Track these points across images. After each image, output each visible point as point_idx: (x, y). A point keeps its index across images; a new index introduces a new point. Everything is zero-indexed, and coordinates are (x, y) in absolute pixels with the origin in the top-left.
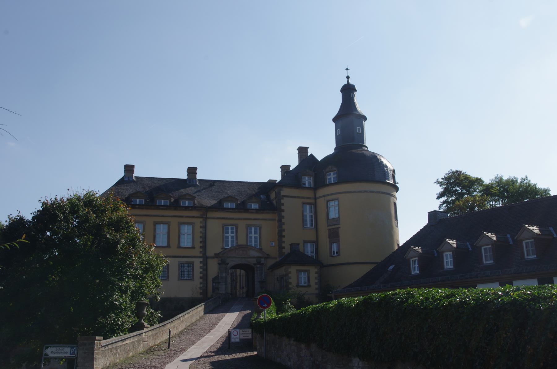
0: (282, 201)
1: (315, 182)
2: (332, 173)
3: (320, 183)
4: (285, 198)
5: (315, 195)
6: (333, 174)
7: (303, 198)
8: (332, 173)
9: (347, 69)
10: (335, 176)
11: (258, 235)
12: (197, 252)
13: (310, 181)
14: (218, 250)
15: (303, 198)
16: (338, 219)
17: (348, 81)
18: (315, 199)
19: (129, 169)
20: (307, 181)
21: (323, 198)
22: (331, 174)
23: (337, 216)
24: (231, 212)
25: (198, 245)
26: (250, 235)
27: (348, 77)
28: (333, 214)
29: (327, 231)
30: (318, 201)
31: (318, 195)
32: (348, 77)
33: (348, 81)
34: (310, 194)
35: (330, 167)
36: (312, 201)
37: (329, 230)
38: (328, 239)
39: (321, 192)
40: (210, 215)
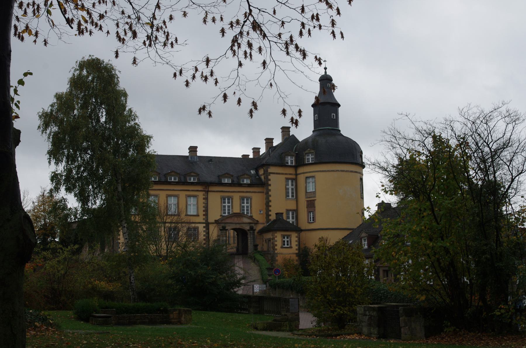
3: (300, 163)
7: (286, 174)
12: (201, 219)
14: (218, 217)
15: (286, 174)
16: (314, 193)
17: (326, 72)
18: (296, 175)
20: (290, 160)
21: (302, 175)
23: (314, 190)
25: (201, 213)
28: (311, 189)
29: (306, 202)
30: (299, 176)
33: (326, 72)
34: (292, 171)
36: (294, 177)
37: (307, 201)
38: (306, 209)
39: (301, 170)
40: (211, 189)
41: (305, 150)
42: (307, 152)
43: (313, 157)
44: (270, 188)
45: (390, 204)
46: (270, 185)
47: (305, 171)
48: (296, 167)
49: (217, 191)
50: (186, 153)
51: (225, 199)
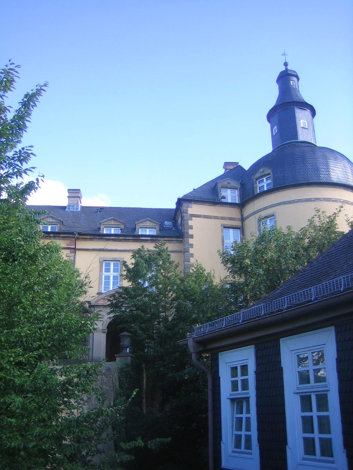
0: (190, 223)
1: (242, 196)
2: (265, 179)
3: (248, 196)
4: (193, 218)
5: (242, 215)
6: (267, 179)
7: (223, 218)
8: (265, 179)
9: (284, 55)
10: (270, 181)
11: (105, 274)
13: (233, 195)
15: (223, 218)
18: (243, 220)
19: (28, 200)
20: (230, 195)
21: (253, 217)
22: (268, 185)
24: (114, 240)
26: (116, 274)
27: (286, 64)
30: (247, 222)
31: (245, 214)
32: (286, 64)
34: (234, 213)
35: (261, 170)
36: (238, 223)
39: (250, 208)
40: (80, 245)
41: (254, 174)
42: (258, 175)
43: (270, 181)
44: (191, 241)
45: (287, 445)
46: (192, 236)
47: (256, 209)
48: (241, 205)
49: (93, 250)
50: (63, 202)
51: (108, 265)
